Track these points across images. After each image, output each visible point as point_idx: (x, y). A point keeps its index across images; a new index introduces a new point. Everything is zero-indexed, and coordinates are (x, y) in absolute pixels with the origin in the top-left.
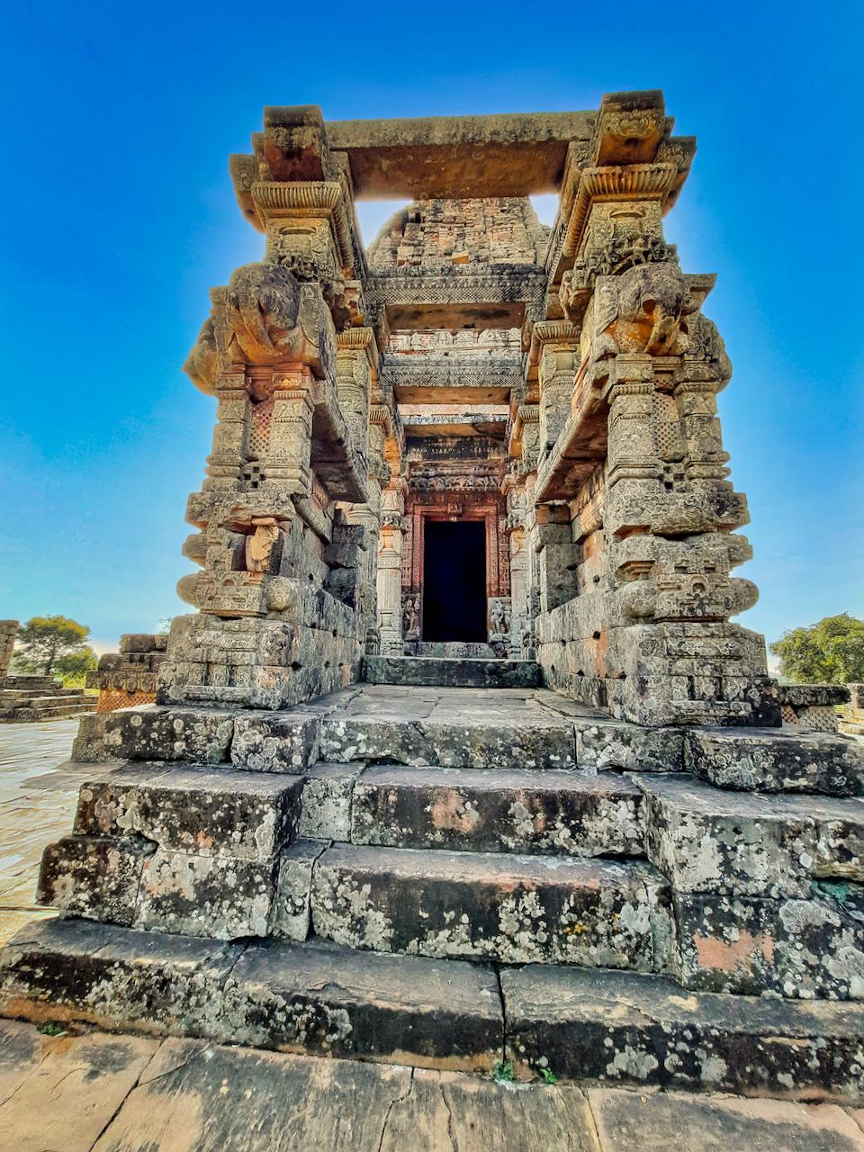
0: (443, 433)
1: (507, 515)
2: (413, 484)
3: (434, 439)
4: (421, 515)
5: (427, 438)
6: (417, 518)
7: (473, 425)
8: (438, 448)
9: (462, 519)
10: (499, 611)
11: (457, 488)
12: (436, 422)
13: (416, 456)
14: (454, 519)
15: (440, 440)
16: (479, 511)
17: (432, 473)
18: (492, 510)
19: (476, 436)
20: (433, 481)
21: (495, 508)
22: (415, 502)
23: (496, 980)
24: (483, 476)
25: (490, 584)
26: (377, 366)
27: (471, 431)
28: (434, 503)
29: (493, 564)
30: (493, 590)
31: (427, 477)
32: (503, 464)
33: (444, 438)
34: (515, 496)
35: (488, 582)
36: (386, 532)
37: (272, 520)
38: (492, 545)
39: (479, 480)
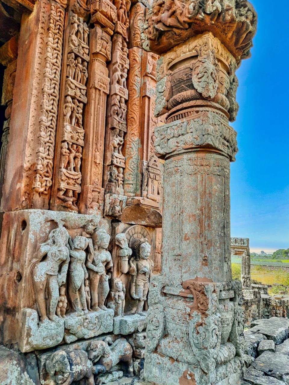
10: (65, 252)
38: (49, 71)
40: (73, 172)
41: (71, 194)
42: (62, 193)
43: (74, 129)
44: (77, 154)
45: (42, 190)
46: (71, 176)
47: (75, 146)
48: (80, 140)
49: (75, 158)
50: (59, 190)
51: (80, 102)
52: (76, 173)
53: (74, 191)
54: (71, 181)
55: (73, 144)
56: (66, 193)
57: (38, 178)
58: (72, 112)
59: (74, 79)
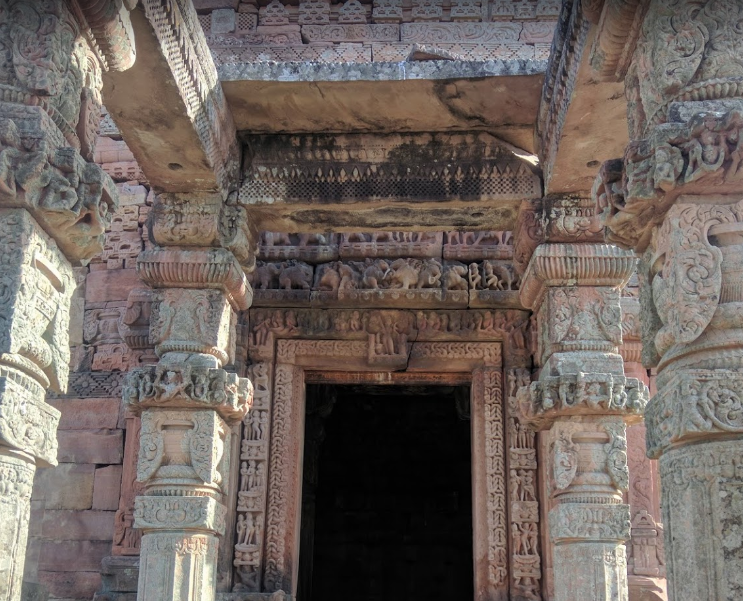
0: (349, 120)
1: (533, 369)
2: (275, 282)
3: (324, 138)
4: (297, 367)
5: (303, 136)
6: (286, 372)
7: (440, 86)
8: (337, 166)
9: (406, 378)
11: (395, 292)
12: (322, 76)
13: (267, 192)
14: (380, 378)
15: (341, 142)
16: (449, 361)
17: (325, 251)
18: (490, 353)
19: (450, 133)
20: (330, 275)
21: (495, 349)
22: (281, 331)
23: (586, 289)
24: (467, 262)
25: (486, 561)
26: (500, 131)
27: (430, 113)
28: (331, 334)
29: (492, 507)
30: (493, 579)
31: (314, 264)
32: (529, 217)
33: (353, 133)
34: (564, 311)
35: (478, 555)
36: (173, 417)
37: (601, 197)
38: (490, 451)
39: (456, 273)
40: (528, 556)
41: (528, 581)
42: (517, 582)
43: (523, 507)
44: (532, 533)
45: (495, 582)
46: (525, 562)
47: (527, 525)
48: (532, 517)
49: (529, 538)
50: (515, 580)
51: (527, 471)
52: (532, 556)
53: (532, 579)
54: (525, 568)
55: (524, 523)
56: (522, 580)
57: (491, 570)
58: (520, 486)
59: (518, 447)
